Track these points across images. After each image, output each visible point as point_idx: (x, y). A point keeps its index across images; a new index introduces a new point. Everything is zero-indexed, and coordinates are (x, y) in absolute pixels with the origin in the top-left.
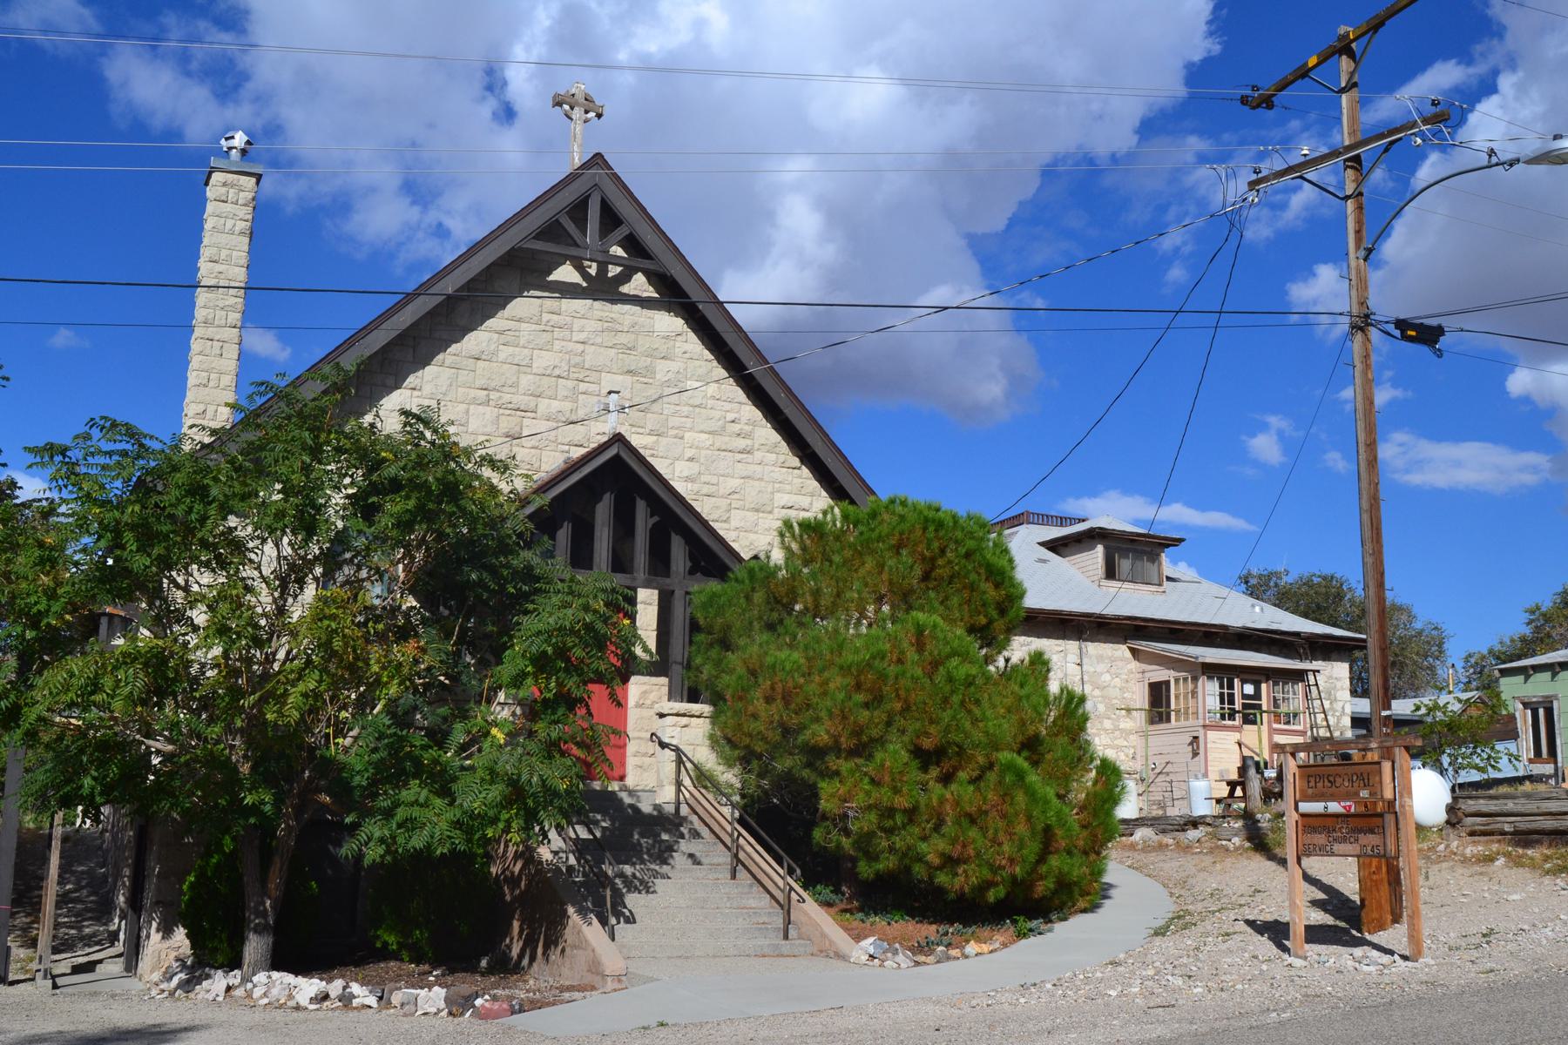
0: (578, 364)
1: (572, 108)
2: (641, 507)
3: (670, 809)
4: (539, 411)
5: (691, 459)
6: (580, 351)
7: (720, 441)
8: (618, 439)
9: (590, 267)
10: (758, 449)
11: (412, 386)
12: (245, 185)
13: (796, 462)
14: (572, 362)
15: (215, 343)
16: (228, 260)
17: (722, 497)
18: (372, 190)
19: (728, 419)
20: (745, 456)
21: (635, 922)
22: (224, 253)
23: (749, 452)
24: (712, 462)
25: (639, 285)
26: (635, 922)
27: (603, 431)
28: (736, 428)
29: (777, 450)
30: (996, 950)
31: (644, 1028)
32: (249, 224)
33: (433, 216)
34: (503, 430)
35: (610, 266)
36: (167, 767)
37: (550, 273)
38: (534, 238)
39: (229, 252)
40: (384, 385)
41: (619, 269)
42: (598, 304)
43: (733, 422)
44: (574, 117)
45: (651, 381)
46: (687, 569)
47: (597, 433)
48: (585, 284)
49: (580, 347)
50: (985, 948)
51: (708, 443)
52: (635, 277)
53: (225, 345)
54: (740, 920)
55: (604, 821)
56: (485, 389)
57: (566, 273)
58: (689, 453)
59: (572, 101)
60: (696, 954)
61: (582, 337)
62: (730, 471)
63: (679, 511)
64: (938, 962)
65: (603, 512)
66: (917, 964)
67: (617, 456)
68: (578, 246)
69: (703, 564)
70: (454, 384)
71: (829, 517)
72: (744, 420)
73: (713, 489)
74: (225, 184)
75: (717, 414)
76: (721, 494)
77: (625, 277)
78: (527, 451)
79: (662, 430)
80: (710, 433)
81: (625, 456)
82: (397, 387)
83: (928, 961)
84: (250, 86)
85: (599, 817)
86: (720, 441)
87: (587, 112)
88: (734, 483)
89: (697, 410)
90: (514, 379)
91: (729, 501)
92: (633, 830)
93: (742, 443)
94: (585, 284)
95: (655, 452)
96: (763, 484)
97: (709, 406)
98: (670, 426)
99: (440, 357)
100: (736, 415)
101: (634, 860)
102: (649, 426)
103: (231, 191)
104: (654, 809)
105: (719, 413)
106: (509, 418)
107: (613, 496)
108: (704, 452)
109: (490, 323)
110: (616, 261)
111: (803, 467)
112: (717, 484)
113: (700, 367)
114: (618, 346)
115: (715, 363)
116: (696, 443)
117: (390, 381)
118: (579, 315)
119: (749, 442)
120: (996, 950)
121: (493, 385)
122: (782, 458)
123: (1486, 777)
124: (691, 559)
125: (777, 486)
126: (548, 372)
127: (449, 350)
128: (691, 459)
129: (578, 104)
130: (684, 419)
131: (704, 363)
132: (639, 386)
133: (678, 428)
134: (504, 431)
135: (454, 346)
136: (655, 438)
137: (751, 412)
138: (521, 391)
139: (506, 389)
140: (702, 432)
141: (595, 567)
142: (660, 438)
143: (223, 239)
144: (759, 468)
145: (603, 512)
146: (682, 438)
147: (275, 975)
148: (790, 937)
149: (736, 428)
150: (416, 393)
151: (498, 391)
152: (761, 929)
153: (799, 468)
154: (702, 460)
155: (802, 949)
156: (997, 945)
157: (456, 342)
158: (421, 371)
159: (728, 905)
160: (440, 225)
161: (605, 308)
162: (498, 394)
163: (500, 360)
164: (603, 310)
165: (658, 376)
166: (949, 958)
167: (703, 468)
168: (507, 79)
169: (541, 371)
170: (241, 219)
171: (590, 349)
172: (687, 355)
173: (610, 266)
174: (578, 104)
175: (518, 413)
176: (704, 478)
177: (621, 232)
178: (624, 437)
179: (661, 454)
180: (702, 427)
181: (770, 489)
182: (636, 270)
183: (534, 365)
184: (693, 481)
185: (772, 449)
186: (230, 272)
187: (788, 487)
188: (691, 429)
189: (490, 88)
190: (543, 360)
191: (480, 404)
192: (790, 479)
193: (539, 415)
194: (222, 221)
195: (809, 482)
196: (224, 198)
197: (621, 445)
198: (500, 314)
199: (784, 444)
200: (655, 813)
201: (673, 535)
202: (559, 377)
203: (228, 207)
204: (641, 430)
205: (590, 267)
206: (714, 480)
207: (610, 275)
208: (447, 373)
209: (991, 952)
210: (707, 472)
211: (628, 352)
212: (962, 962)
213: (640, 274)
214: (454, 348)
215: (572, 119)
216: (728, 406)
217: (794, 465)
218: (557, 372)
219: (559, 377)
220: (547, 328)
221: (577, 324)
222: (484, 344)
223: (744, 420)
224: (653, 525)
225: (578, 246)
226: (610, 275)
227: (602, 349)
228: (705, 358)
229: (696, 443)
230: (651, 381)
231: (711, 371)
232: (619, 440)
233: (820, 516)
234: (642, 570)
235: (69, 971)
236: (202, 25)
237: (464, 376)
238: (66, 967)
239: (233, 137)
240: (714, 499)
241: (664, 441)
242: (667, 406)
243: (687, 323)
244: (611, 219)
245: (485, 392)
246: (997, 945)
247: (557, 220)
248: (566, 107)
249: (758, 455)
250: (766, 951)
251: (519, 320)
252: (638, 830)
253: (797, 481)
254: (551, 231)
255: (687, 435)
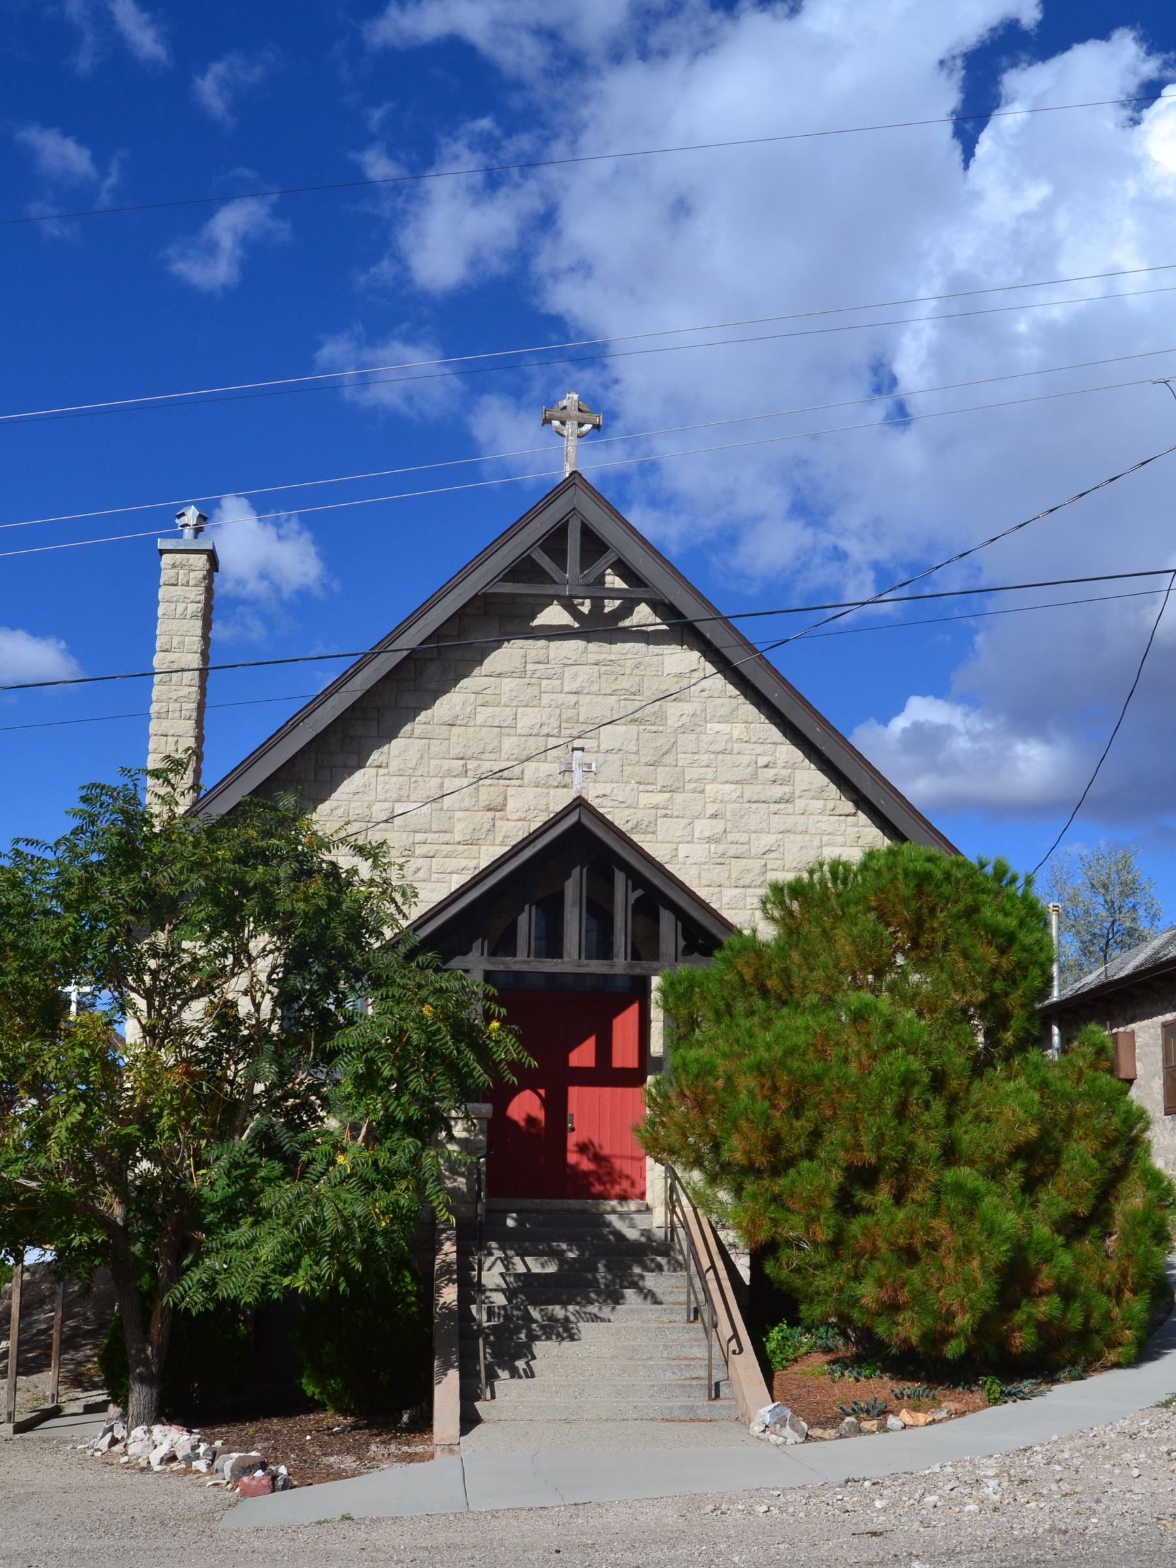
0: (571, 718)
1: (563, 423)
2: (620, 877)
3: (660, 1234)
4: (526, 777)
5: (714, 816)
6: (572, 703)
7: (750, 791)
8: (580, 803)
9: (582, 604)
10: (800, 797)
11: (377, 763)
12: (195, 564)
13: (849, 807)
14: (564, 717)
15: (170, 738)
16: (181, 647)
17: (755, 857)
18: (757, 519)
19: (760, 764)
20: (781, 806)
21: (533, 1376)
22: (176, 640)
23: (787, 801)
24: (741, 817)
25: (643, 615)
26: (533, 1376)
27: (603, 792)
28: (771, 773)
29: (825, 794)
30: (940, 1421)
31: (319, 1523)
32: (201, 605)
33: (827, 540)
34: (482, 804)
35: (606, 601)
36: (11, 1207)
37: (534, 618)
38: (500, 580)
39: (180, 639)
40: (345, 766)
41: (618, 603)
42: (593, 646)
43: (766, 766)
44: (565, 433)
45: (661, 728)
46: (680, 949)
47: (561, 800)
48: (576, 625)
49: (573, 698)
50: (922, 1418)
51: (734, 795)
52: (637, 609)
53: (180, 739)
54: (668, 1374)
55: (571, 1250)
56: (462, 759)
57: (554, 615)
58: (711, 809)
59: (563, 414)
60: (586, 1416)
61: (574, 686)
62: (764, 825)
63: (657, 881)
64: (841, 1437)
65: (573, 889)
66: (808, 1438)
67: (578, 825)
68: (554, 582)
69: (701, 941)
70: (426, 756)
71: (816, 877)
72: (780, 763)
73: (742, 849)
74: (174, 566)
75: (745, 759)
76: (753, 853)
77: (627, 610)
78: (511, 824)
79: (676, 784)
80: (737, 783)
81: (587, 822)
82: (361, 765)
83: (826, 1436)
84: (619, 425)
85: (564, 1246)
86: (750, 791)
87: (581, 425)
88: (768, 840)
89: (720, 757)
90: (495, 743)
91: (763, 862)
92: (596, 1264)
93: (778, 791)
94: (576, 625)
95: (669, 812)
96: (807, 837)
97: (735, 751)
98: (687, 778)
99: (408, 728)
100: (770, 758)
101: (579, 1299)
102: (660, 783)
103: (181, 572)
104: (642, 1235)
105: (748, 757)
106: (491, 788)
107: (585, 870)
108: (729, 807)
109: (464, 682)
110: (614, 594)
111: (860, 813)
112: (748, 843)
113: (722, 705)
114: (622, 693)
115: (741, 699)
116: (720, 797)
117: (352, 761)
118: (570, 662)
119: (787, 789)
120: (940, 1421)
121: (469, 753)
122: (831, 804)
123: (919, 1250)
124: (685, 938)
125: (825, 838)
126: (535, 731)
127: (418, 719)
128: (714, 816)
129: (570, 418)
130: (704, 770)
131: (727, 700)
132: (646, 736)
133: (697, 781)
134: (484, 804)
135: (423, 713)
136: (668, 795)
137: (789, 752)
138: (504, 756)
139: (485, 756)
140: (727, 782)
141: (565, 954)
142: (675, 795)
143: (174, 625)
144: (801, 820)
145: (573, 889)
146: (702, 792)
147: (157, 1429)
148: (722, 1395)
149: (771, 773)
150: (382, 771)
151: (476, 759)
152: (683, 1386)
153: (855, 815)
154: (728, 816)
155: (724, 1412)
156: (944, 1414)
157: (426, 709)
158: (386, 747)
159: (665, 1355)
160: (836, 548)
161: (603, 650)
162: (476, 763)
163: (478, 723)
164: (598, 653)
165: (670, 722)
166: (860, 1431)
167: (729, 825)
168: (898, 376)
169: (526, 731)
170: (192, 602)
171: (584, 699)
172: (706, 694)
173: (606, 601)
174: (570, 418)
175: (501, 782)
176: (730, 837)
177: (610, 557)
178: (586, 801)
179: (676, 814)
180: (727, 777)
181: (816, 843)
182: (638, 602)
183: (519, 725)
184: (717, 841)
185: (820, 794)
186: (183, 660)
187: (840, 839)
188: (714, 780)
189: (878, 390)
190: (528, 719)
191: (455, 776)
192: (843, 828)
193: (526, 781)
194: (173, 606)
195: (868, 830)
196: (173, 581)
197: (583, 810)
198: (476, 671)
199: (833, 787)
200: (643, 1239)
201: (662, 910)
202: (548, 735)
203: (179, 590)
204: (650, 788)
205: (582, 604)
206: (744, 838)
207: (607, 610)
208: (416, 745)
209: (930, 1423)
210: (735, 830)
211: (632, 697)
212: (879, 1437)
213: (643, 604)
214: (423, 716)
215: (564, 436)
216: (759, 749)
217: (846, 811)
218: (545, 730)
219: (548, 735)
220: (534, 681)
221: (568, 671)
222: (458, 708)
223: (780, 763)
224: (637, 900)
225: (554, 582)
226: (607, 610)
227: (600, 698)
228: (728, 694)
229: (720, 797)
230: (661, 728)
231: (737, 709)
232: (579, 805)
233: (805, 876)
234: (622, 954)
235: (81, 1411)
236: (560, 366)
237: (435, 746)
238: (78, 1406)
239: (183, 514)
240: (745, 860)
241: (679, 797)
242: (683, 755)
243: (704, 655)
244: (594, 545)
245: (461, 762)
246: (944, 1414)
247: (529, 555)
248: (556, 423)
249: (800, 804)
250: (677, 1413)
251: (500, 675)
252: (604, 1262)
253: (852, 831)
254: (523, 570)
255: (709, 788)
